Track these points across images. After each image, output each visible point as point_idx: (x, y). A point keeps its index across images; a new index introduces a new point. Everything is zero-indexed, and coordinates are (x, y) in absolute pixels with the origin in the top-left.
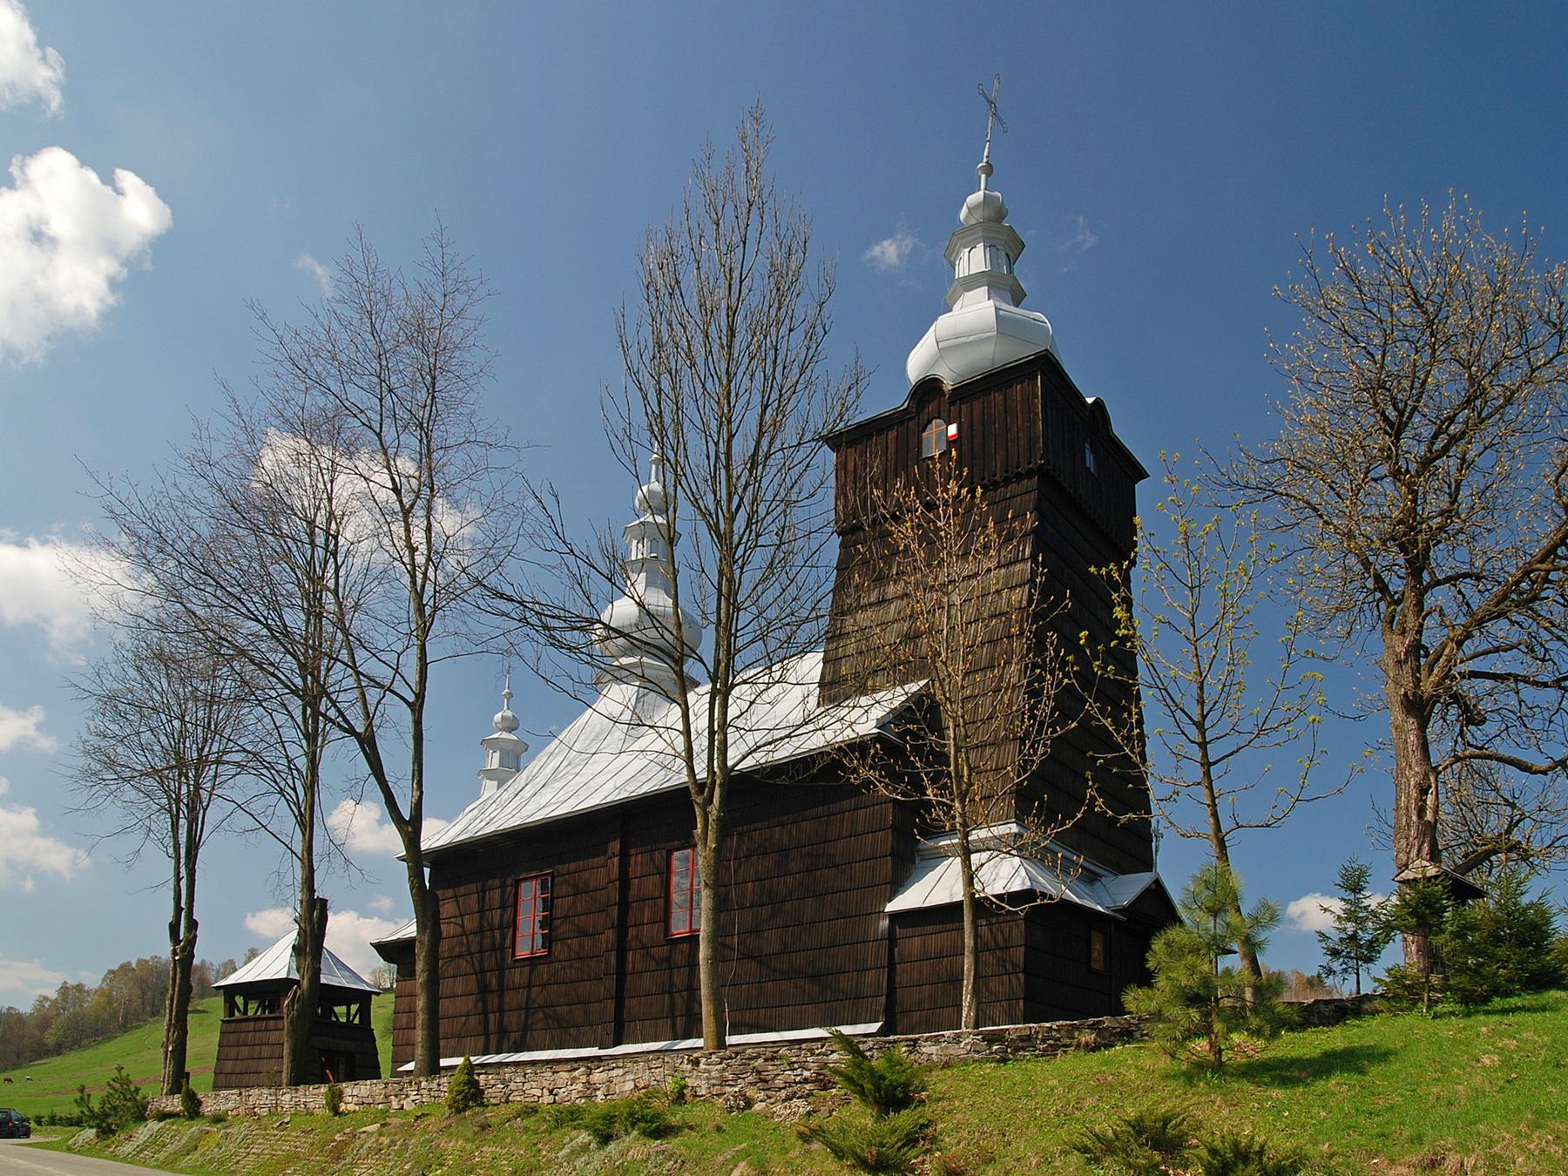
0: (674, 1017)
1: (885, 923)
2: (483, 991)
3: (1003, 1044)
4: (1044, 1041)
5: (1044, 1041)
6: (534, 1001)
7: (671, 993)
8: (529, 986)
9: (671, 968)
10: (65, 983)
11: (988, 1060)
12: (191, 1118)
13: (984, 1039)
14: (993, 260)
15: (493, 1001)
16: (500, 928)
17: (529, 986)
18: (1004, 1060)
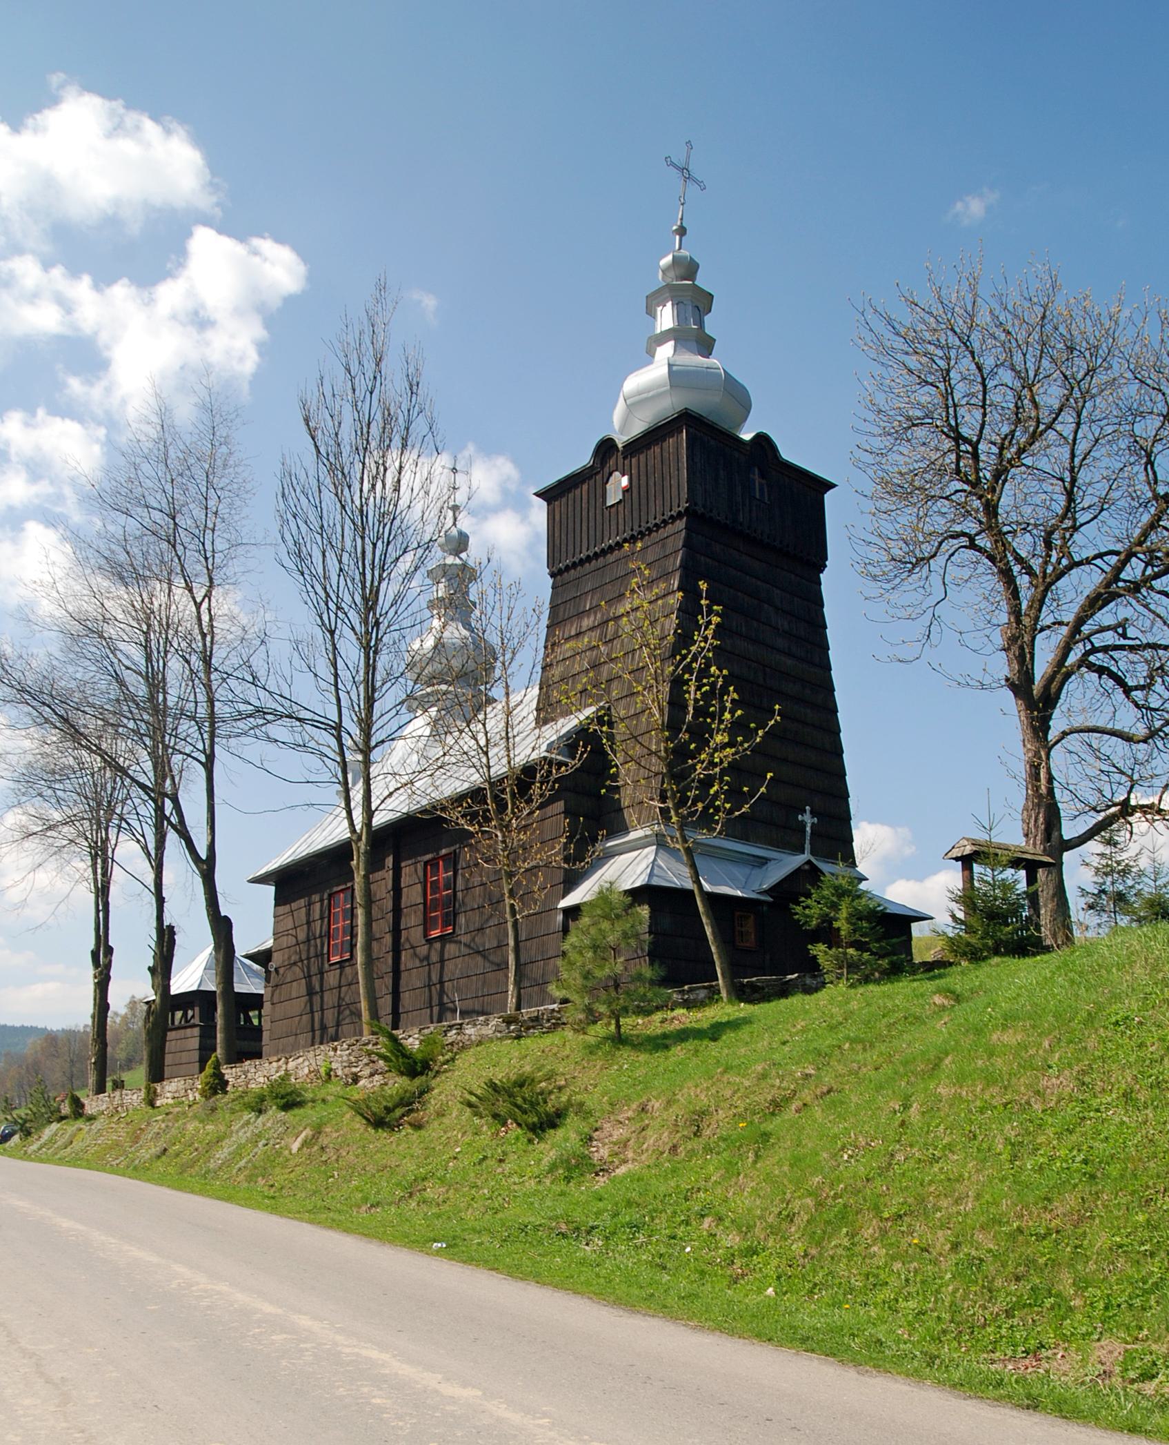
0: (431, 1007)
1: (560, 917)
2: (310, 993)
3: (517, 1024)
4: (548, 1021)
5: (548, 1021)
6: (343, 1000)
7: (429, 986)
8: (340, 987)
9: (429, 965)
10: (133, 997)
11: (507, 1038)
12: (76, 1118)
13: (503, 1021)
14: (680, 316)
15: (317, 999)
16: (321, 936)
17: (340, 987)
18: (518, 1037)
